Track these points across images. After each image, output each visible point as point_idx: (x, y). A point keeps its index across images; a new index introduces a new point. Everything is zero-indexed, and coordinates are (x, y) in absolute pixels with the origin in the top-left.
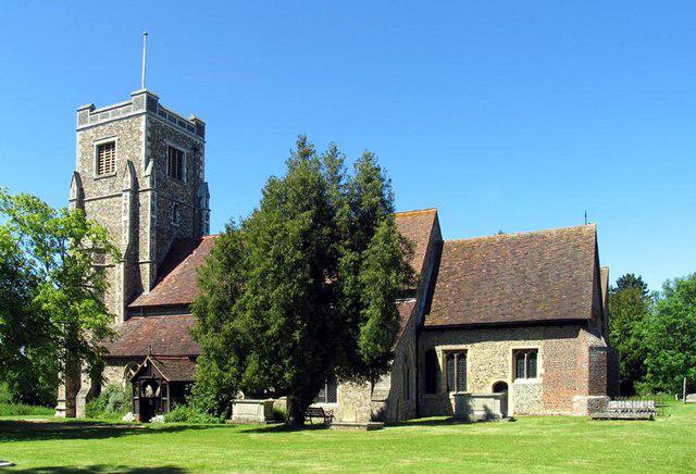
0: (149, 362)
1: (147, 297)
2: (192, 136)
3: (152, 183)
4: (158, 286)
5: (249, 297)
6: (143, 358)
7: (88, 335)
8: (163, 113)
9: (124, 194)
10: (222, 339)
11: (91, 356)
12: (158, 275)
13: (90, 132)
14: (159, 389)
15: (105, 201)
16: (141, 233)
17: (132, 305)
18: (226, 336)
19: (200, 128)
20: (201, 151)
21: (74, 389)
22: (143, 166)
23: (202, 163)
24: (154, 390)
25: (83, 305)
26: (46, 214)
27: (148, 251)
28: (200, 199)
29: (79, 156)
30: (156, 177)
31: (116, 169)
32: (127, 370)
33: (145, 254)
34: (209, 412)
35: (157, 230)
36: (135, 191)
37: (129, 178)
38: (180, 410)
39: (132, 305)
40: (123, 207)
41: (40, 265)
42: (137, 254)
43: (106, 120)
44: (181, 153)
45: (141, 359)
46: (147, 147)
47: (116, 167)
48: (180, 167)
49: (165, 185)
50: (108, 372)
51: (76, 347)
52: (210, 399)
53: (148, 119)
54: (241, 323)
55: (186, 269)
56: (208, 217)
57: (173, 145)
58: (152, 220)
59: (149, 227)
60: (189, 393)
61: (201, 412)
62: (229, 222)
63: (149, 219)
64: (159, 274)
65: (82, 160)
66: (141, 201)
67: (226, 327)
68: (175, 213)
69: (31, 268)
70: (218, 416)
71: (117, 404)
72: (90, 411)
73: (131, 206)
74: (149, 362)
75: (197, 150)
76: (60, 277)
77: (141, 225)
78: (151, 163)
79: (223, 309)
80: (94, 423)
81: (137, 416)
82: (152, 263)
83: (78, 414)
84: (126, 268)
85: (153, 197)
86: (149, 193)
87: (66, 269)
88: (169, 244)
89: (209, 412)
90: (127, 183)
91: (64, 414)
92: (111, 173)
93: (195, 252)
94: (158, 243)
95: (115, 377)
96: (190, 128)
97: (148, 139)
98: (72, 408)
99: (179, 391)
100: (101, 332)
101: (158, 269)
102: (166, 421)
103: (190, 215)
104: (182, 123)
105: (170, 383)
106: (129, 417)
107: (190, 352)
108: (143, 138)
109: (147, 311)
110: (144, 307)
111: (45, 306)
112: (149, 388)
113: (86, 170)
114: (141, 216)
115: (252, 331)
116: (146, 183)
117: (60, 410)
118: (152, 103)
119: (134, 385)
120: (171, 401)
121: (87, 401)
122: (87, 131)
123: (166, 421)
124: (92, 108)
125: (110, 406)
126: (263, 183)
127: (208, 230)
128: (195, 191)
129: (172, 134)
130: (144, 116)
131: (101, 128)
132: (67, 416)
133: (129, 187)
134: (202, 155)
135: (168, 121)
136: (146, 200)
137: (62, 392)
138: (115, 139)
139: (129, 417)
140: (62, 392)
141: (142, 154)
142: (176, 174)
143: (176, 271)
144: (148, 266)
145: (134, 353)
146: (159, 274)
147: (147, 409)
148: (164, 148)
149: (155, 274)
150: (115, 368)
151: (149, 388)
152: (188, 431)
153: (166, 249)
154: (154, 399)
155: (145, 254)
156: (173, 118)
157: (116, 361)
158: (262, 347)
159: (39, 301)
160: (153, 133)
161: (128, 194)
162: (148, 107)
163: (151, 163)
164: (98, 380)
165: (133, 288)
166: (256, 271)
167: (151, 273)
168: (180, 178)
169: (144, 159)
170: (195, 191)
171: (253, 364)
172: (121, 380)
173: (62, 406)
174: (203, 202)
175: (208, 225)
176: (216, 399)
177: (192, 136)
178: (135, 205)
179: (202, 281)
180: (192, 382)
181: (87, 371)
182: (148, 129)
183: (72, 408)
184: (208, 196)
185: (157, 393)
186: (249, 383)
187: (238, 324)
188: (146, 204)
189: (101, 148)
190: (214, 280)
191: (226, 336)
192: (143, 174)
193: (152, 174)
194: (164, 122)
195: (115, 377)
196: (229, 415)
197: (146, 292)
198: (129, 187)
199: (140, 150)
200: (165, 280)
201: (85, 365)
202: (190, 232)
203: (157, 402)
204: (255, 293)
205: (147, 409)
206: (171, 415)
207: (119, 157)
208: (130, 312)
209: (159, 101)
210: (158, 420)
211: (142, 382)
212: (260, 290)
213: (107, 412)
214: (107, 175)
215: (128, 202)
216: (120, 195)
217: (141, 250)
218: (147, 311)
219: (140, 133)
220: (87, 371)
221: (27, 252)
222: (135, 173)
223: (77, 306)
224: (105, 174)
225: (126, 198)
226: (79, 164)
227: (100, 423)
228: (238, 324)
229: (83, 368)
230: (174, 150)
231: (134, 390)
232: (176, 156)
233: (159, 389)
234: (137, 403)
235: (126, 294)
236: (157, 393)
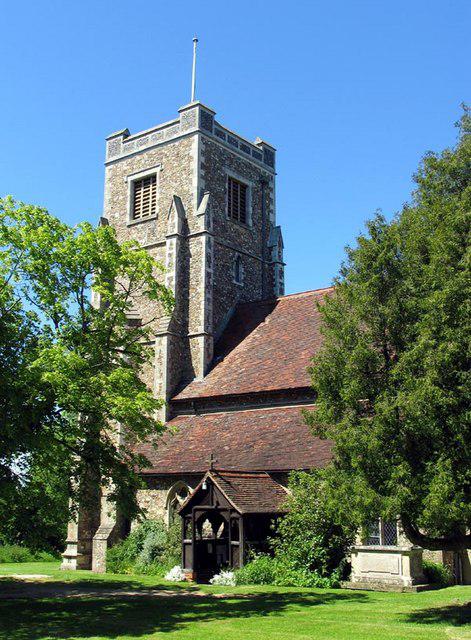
0: (210, 483)
1: (201, 385)
2: (259, 164)
3: (208, 224)
4: (216, 369)
5: (427, 347)
6: (200, 476)
7: (114, 434)
8: (221, 133)
9: (168, 241)
10: (378, 429)
11: (121, 472)
12: (216, 354)
13: (124, 165)
14: (222, 527)
15: (152, 152)
16: (192, 293)
17: (181, 396)
18: (385, 422)
19: (268, 155)
20: (271, 185)
21: (91, 525)
22: (195, 202)
23: (272, 201)
24: (215, 528)
25: (112, 377)
26: (56, 231)
27: (202, 318)
28: (271, 249)
29: (107, 196)
30: (212, 218)
31: (157, 211)
32: (171, 496)
33: (198, 322)
34: (312, 568)
35: (214, 290)
36: (184, 236)
37: (175, 219)
38: (260, 561)
39: (181, 396)
40: (167, 260)
41: (44, 320)
42: (186, 324)
43: (144, 147)
44: (244, 187)
45: (194, 478)
46: (201, 177)
47: (157, 207)
48: (244, 205)
49: (224, 229)
50: (143, 497)
51: (98, 456)
52: (312, 543)
53: (202, 139)
54: (413, 399)
55: (257, 343)
56: (282, 273)
57: (234, 176)
58: (208, 275)
59: (203, 285)
60: (274, 535)
61: (297, 567)
62: (373, 218)
63: (203, 274)
64: (218, 351)
65: (112, 201)
66: (193, 250)
67: (384, 406)
68: (237, 266)
69: (30, 324)
70: (328, 575)
71: (156, 552)
72: (114, 563)
73: (178, 256)
74: (210, 483)
75: (266, 183)
76: (75, 339)
77: (192, 282)
78: (206, 198)
79: (374, 380)
80: (119, 586)
81: (189, 570)
82: (206, 335)
83: (96, 564)
84: (170, 343)
85: (208, 243)
86: (203, 239)
87: (85, 322)
88: (230, 310)
89: (312, 568)
90: (173, 225)
91: (74, 563)
92: (151, 216)
93: (267, 320)
94: (215, 307)
95: (155, 505)
96: (257, 155)
97: (202, 166)
98: (86, 564)
99: (260, 531)
100: (138, 425)
101: (215, 345)
102: (239, 583)
103: (257, 267)
104: (246, 147)
105: (247, 517)
106: (176, 575)
107: (280, 464)
108: (194, 165)
109: (201, 405)
110: (195, 400)
111: (45, 377)
112: (207, 525)
113: (117, 215)
114: (192, 271)
115: (439, 414)
116: (198, 225)
117: (70, 558)
118: (207, 119)
119: (186, 520)
120: (246, 547)
121: (109, 546)
122: (119, 164)
123: (239, 583)
124: (126, 134)
125: (145, 554)
126: (415, 164)
127: (282, 292)
128: (264, 240)
129: (232, 161)
130: (196, 137)
131: (138, 157)
132: (81, 567)
133: (176, 231)
134: (272, 190)
135: (226, 143)
136: (199, 248)
137: (72, 531)
138: (157, 170)
139: (176, 575)
140: (72, 531)
141: (193, 185)
142: (239, 214)
143: (242, 347)
144: (201, 340)
145: (181, 469)
146: (218, 351)
147: (206, 562)
148: (222, 179)
149: (211, 351)
150: (154, 492)
151: (207, 525)
152: (294, 611)
153: (226, 317)
154: (215, 542)
155: (198, 322)
156: (233, 140)
157: (156, 481)
158: (456, 444)
159: (36, 368)
160: (208, 160)
161: (174, 240)
162: (202, 125)
163: (206, 198)
164: (128, 509)
165: (180, 374)
166: (434, 299)
167: (207, 349)
168: (244, 220)
169: (196, 195)
170: (264, 240)
171: (440, 484)
172: (160, 512)
173: (72, 551)
174: (275, 252)
175: (282, 284)
176: (325, 544)
177: (259, 164)
178: (184, 255)
179: (333, 321)
180: (282, 515)
181: (111, 498)
182: (202, 153)
183: (86, 564)
184: (281, 245)
185: (219, 534)
186: (438, 520)
187: (409, 401)
188: (199, 254)
189: (137, 184)
190: (352, 317)
191: (385, 422)
192: (195, 213)
193: (207, 213)
194: (222, 145)
195: (155, 505)
196: (347, 571)
197: (199, 378)
198: (176, 231)
199: (191, 180)
200: (226, 360)
201: (110, 489)
202: (257, 294)
203: (219, 548)
204: (437, 336)
205: (206, 562)
206: (246, 571)
207: (162, 194)
208: (176, 408)
209: (216, 118)
210: (225, 583)
211: (198, 515)
212: (448, 332)
213: (139, 562)
214: (146, 218)
215: (174, 252)
216: (163, 244)
217: (192, 318)
218: (201, 405)
219: (190, 158)
220: (111, 498)
221: (28, 304)
222: (184, 211)
223: (100, 378)
224: (142, 219)
225: (172, 247)
226: (107, 207)
227: (128, 585)
228: (409, 401)
229: (106, 491)
230: (236, 183)
231: (185, 528)
232: (238, 191)
233: (222, 527)
234: (190, 551)
235: (170, 382)
236: (219, 534)
